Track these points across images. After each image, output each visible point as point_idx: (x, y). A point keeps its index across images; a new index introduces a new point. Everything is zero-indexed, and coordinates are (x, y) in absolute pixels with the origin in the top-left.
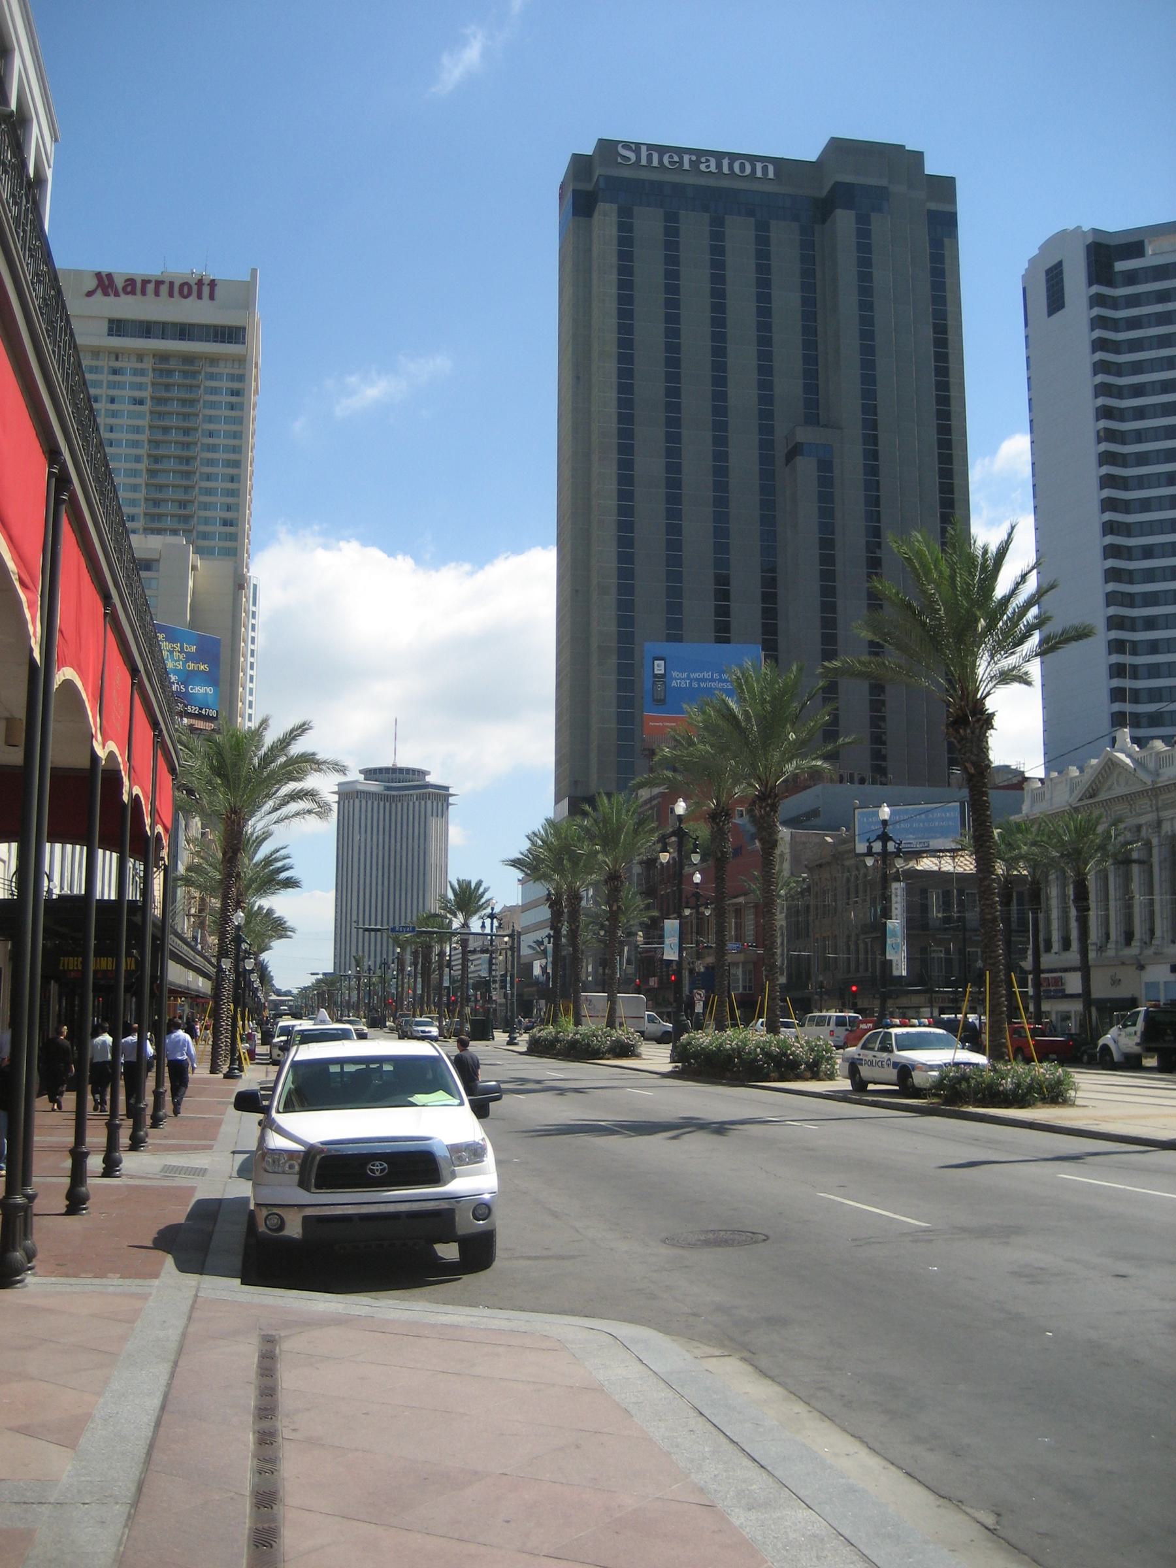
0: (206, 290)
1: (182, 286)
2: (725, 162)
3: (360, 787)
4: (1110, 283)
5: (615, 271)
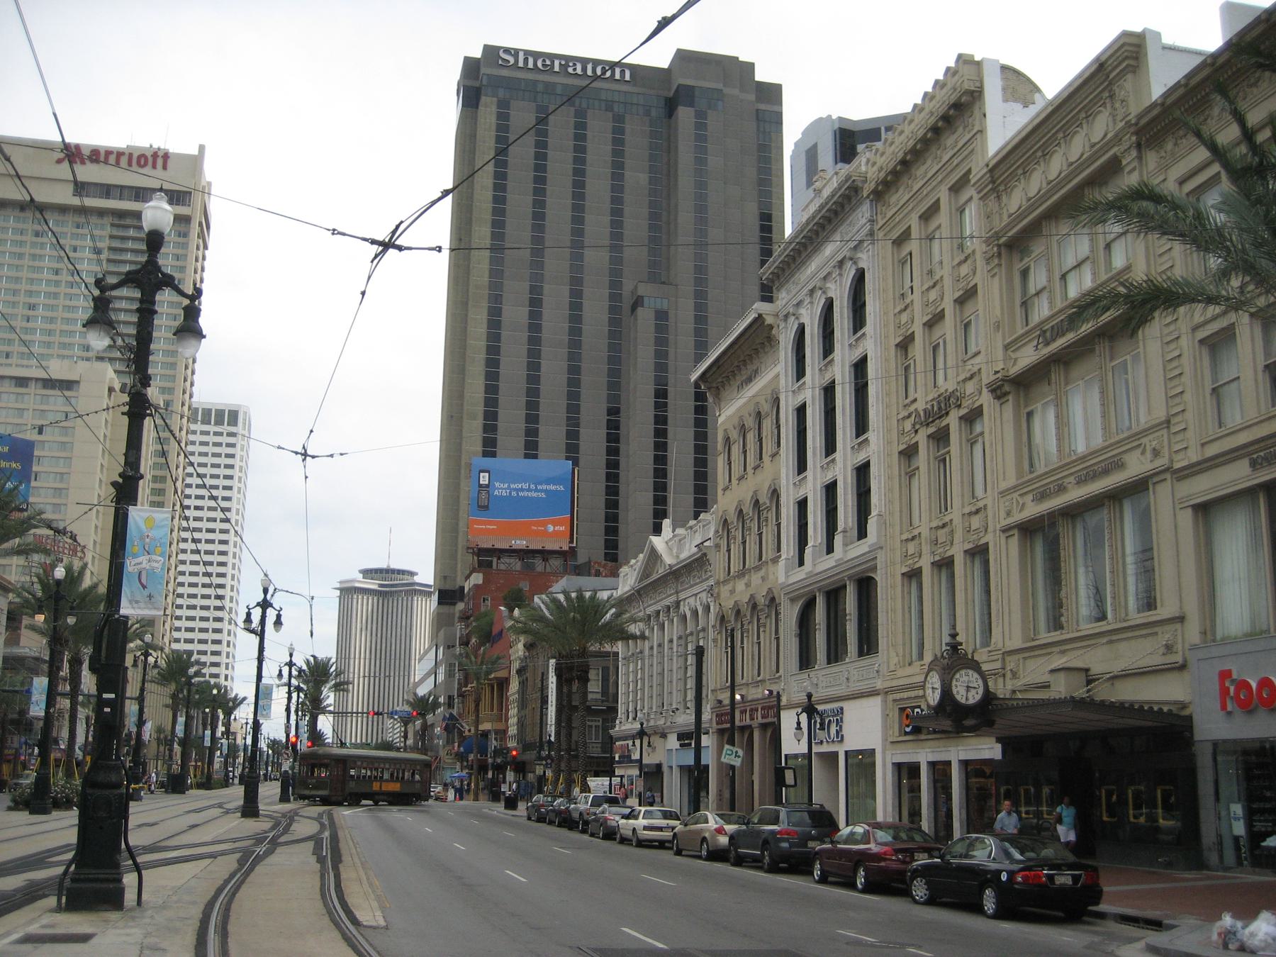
0: (160, 162)
1: (139, 157)
2: (590, 67)
3: (357, 585)
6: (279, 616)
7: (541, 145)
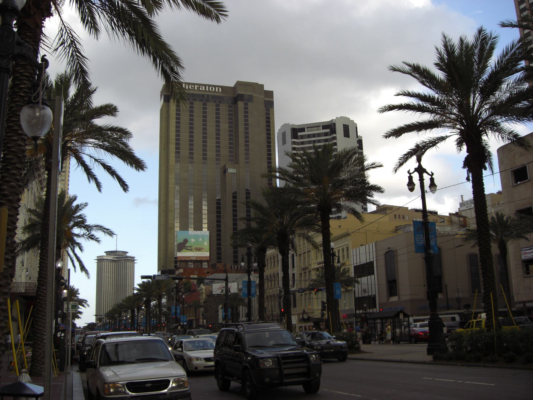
2: (207, 87)
3: (104, 258)
4: (297, 138)
5: (175, 119)
6: (432, 180)
7: (235, 215)
